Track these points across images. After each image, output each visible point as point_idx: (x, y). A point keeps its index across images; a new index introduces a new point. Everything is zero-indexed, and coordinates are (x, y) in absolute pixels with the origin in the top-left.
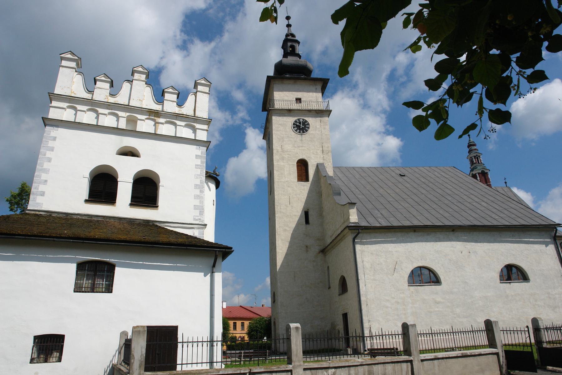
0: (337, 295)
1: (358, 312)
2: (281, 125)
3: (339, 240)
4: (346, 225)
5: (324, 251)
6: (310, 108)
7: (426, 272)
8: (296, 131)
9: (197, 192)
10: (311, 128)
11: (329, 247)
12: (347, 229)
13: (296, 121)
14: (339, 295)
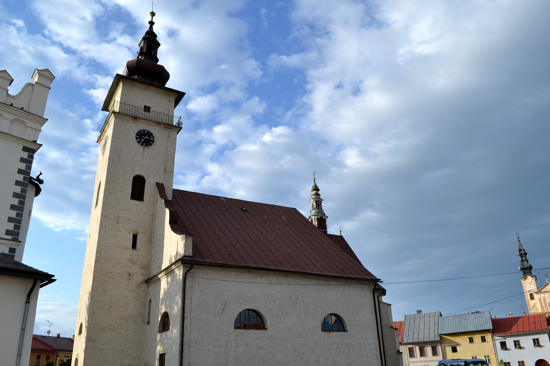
7: (334, 318)
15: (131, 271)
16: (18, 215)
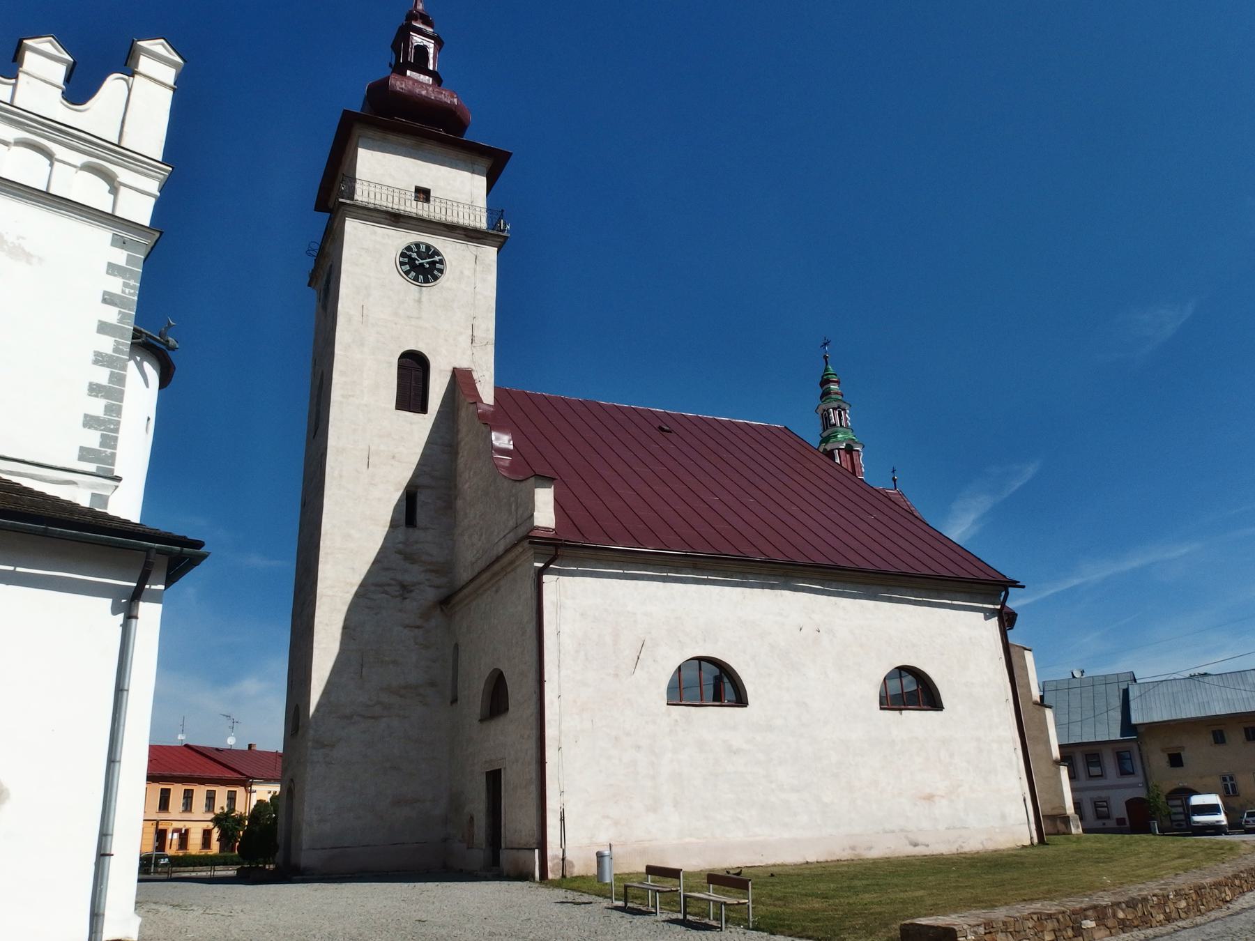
0: (476, 722)
3: (503, 569)
4: (522, 531)
5: (446, 602)
6: (452, 218)
8: (407, 273)
9: (102, 376)
11: (466, 591)
12: (526, 544)
13: (409, 248)
14: (482, 720)
15: (408, 578)
16: (108, 409)
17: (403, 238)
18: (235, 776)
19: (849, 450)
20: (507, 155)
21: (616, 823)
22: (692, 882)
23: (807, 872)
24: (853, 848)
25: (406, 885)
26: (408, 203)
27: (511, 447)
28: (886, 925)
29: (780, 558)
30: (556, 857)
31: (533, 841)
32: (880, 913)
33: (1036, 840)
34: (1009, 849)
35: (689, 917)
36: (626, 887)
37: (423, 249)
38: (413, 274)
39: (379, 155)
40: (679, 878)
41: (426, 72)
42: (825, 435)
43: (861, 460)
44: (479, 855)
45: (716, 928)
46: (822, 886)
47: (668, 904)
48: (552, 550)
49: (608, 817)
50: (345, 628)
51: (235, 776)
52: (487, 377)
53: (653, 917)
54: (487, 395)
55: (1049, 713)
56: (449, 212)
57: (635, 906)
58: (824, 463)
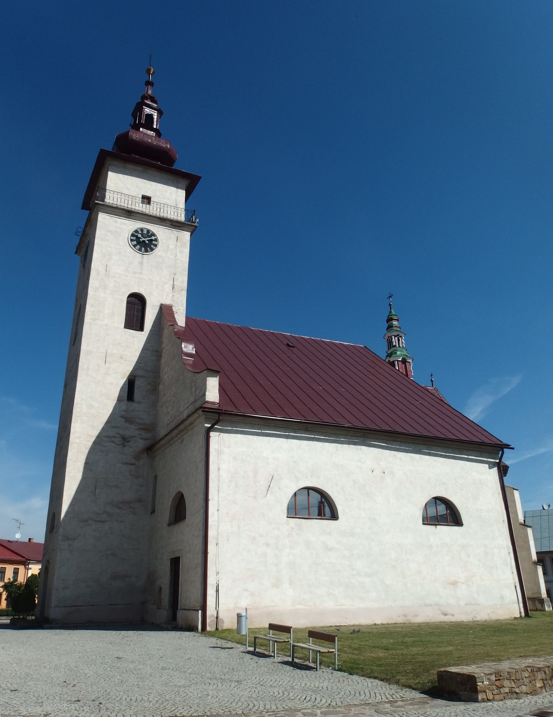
1: (200, 557)
2: (111, 232)
3: (186, 428)
4: (198, 404)
5: (150, 449)
8: (135, 246)
10: (159, 246)
11: (163, 442)
12: (200, 412)
13: (136, 231)
14: (169, 525)
17: (132, 225)
18: (19, 558)
19: (404, 361)
20: (198, 178)
21: (252, 594)
22: (300, 635)
23: (375, 630)
24: (405, 616)
25: (115, 632)
26: (137, 205)
27: (194, 352)
28: (428, 671)
29: (360, 425)
30: (213, 616)
31: (198, 604)
32: (423, 662)
33: (523, 614)
34: (506, 620)
35: (296, 660)
36: (255, 638)
37: (145, 232)
38: (138, 247)
39: (121, 176)
40: (289, 632)
41: (152, 129)
42: (389, 352)
43: (411, 368)
44: (163, 614)
45: (313, 668)
46: (384, 641)
47: (282, 650)
48: (216, 416)
49: (247, 590)
50: (86, 463)
51: (19, 558)
52: (181, 310)
53: (272, 659)
54: (181, 320)
55: (530, 531)
56: (162, 211)
57: (261, 651)
58: (387, 370)
